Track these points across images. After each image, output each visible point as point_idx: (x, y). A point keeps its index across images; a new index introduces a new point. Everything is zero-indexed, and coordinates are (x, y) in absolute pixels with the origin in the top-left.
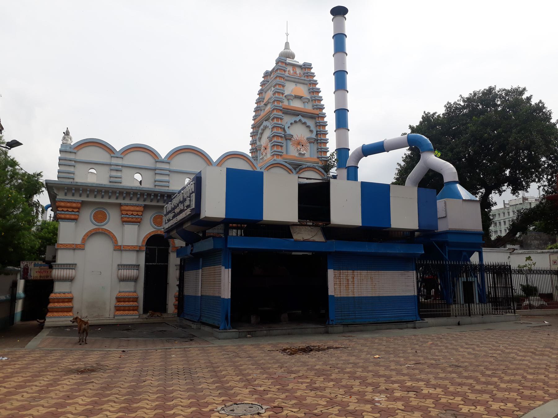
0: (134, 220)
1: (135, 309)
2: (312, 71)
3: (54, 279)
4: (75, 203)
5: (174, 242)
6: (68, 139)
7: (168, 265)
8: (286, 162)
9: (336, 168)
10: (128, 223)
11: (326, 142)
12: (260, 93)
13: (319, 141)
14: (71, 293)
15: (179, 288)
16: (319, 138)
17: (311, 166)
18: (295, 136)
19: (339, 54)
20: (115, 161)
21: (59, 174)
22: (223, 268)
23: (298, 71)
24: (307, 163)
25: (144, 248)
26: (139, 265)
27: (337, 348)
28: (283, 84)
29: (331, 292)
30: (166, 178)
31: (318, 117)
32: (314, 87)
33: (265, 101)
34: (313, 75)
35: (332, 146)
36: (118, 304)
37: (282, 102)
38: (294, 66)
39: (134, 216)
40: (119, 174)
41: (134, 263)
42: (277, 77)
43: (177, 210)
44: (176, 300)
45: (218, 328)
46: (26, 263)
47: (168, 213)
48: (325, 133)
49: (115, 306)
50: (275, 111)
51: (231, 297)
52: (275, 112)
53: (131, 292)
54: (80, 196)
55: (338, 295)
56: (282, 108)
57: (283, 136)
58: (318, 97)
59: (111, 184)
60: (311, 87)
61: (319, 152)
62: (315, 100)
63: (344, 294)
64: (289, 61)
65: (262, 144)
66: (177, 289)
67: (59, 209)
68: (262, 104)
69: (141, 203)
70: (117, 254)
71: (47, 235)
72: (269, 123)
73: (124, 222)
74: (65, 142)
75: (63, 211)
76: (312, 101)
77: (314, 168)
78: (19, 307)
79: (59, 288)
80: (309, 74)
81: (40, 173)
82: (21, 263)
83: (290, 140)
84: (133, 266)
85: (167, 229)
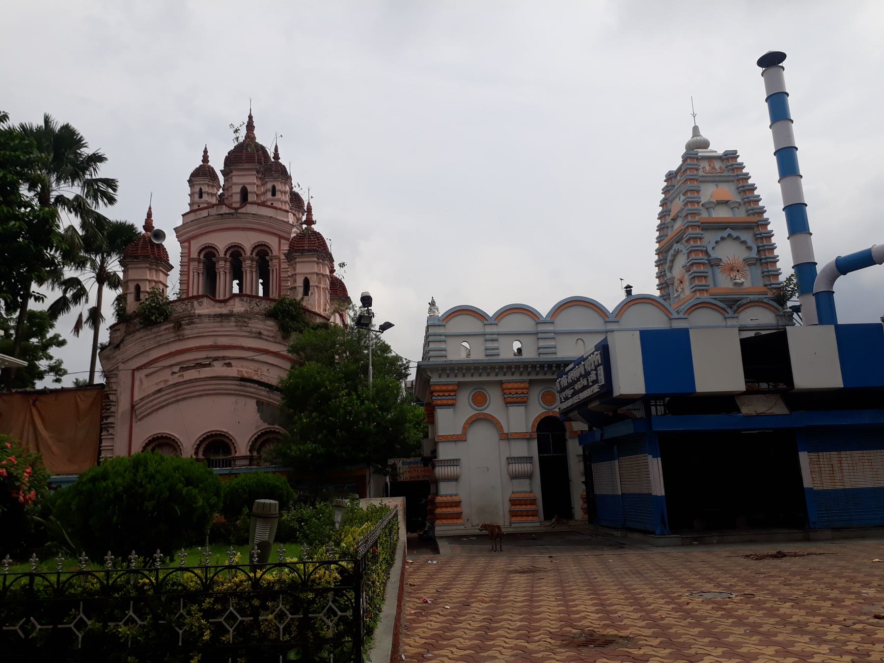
0: (519, 400)
1: (534, 514)
2: (739, 160)
4: (450, 385)
5: (571, 425)
7: (566, 456)
8: (715, 299)
9: (797, 294)
10: (513, 405)
11: (775, 259)
12: (663, 203)
13: (763, 261)
14: (456, 495)
15: (586, 486)
16: (763, 257)
17: (756, 300)
18: (724, 259)
19: (779, 124)
20: (489, 329)
22: (650, 457)
23: (718, 165)
24: (748, 296)
25: (535, 435)
26: (532, 457)
27: (820, 554)
28: (697, 188)
29: (807, 483)
30: (551, 343)
31: (758, 226)
32: (745, 184)
33: (673, 214)
34: (741, 166)
35: (786, 265)
36: (513, 507)
37: (699, 214)
38: (710, 159)
39: (518, 395)
40: (495, 345)
41: (526, 454)
42: (686, 181)
43: (578, 386)
44: (584, 502)
45: (653, 533)
47: (563, 390)
48: (772, 248)
49: (510, 511)
50: (690, 229)
51: (665, 493)
52: (690, 230)
53: (524, 492)
54: (456, 376)
55: (818, 487)
56: (699, 223)
57: (707, 262)
58: (753, 197)
59: (487, 358)
60: (741, 185)
61: (765, 277)
62: (749, 202)
63: (828, 485)
64: (701, 153)
65: (674, 275)
66: (584, 487)
68: (668, 219)
69: (525, 377)
70: (504, 444)
72: (682, 245)
73: (507, 403)
75: (439, 396)
76: (744, 204)
77: (761, 302)
79: (445, 490)
80: (735, 166)
83: (718, 265)
84: (525, 459)
85: (564, 409)
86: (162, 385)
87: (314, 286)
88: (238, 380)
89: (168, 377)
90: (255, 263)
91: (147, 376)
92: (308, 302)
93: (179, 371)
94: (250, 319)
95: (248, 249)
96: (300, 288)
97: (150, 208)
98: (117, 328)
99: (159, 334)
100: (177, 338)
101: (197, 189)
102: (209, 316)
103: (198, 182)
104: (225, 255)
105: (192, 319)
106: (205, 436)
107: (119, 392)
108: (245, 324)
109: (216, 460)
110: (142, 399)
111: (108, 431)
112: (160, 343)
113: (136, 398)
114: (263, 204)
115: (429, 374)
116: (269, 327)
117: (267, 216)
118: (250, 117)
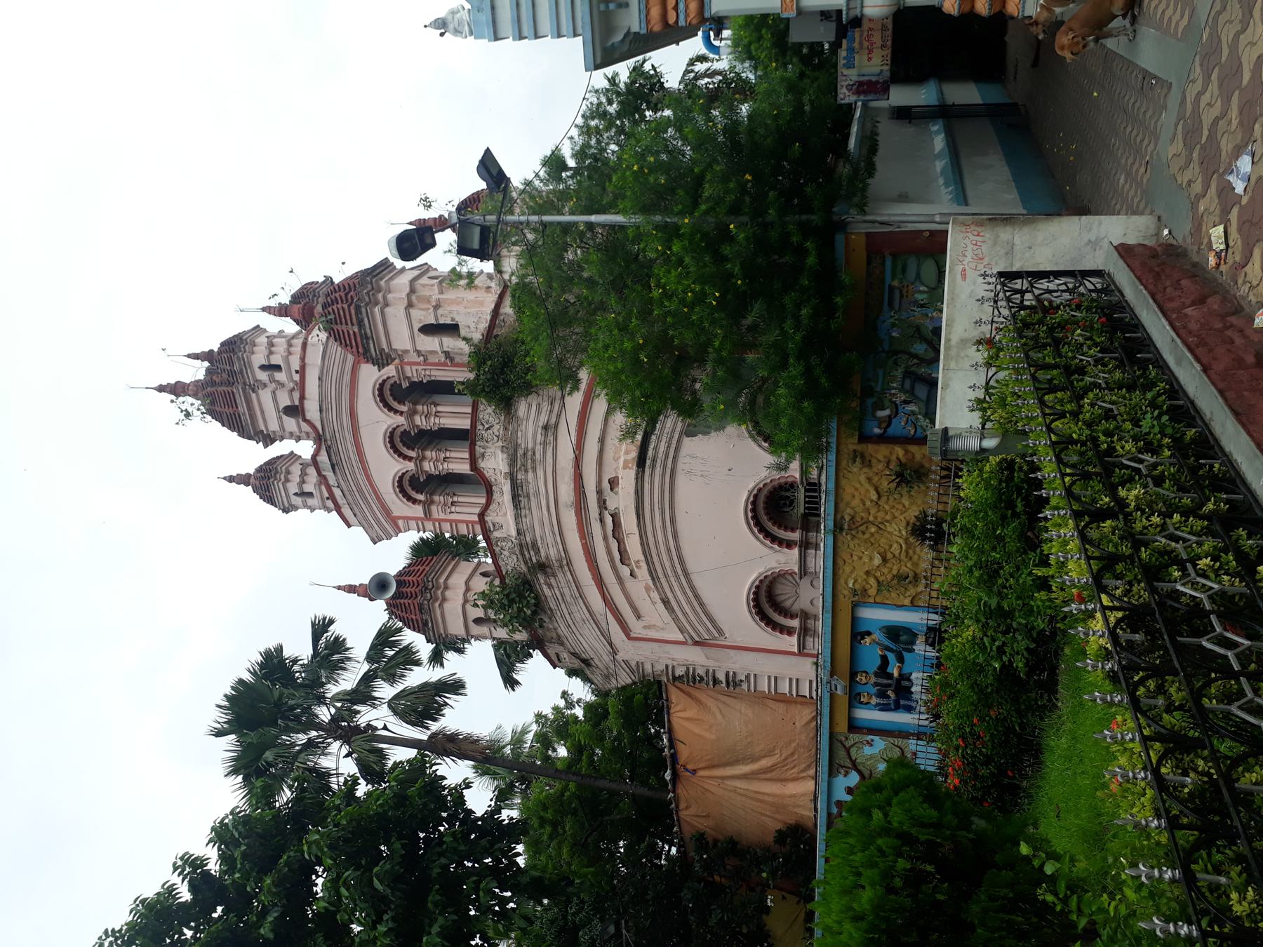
3: (894, 9)
6: (456, 20)
21: (526, 35)
46: (844, 90)
67: (671, 21)
71: (767, 44)
74: (466, 28)
78: (965, 94)
81: (609, 80)
82: (843, 102)
86: (655, 595)
87: (436, 316)
88: (644, 471)
89: (640, 586)
90: (419, 408)
91: (639, 617)
92: (472, 329)
93: (628, 565)
94: (517, 446)
95: (393, 421)
96: (445, 345)
97: (339, 588)
98: (554, 658)
99: (560, 598)
100: (566, 568)
101: (297, 501)
102: (518, 517)
103: (285, 499)
104: (410, 459)
105: (525, 546)
106: (756, 530)
107: (670, 663)
108: (530, 453)
109: (806, 502)
110: (682, 630)
111: (741, 681)
112: (577, 595)
113: (680, 637)
114: (302, 385)
115: (618, 37)
116: (530, 411)
117: (320, 386)
118: (161, 389)
